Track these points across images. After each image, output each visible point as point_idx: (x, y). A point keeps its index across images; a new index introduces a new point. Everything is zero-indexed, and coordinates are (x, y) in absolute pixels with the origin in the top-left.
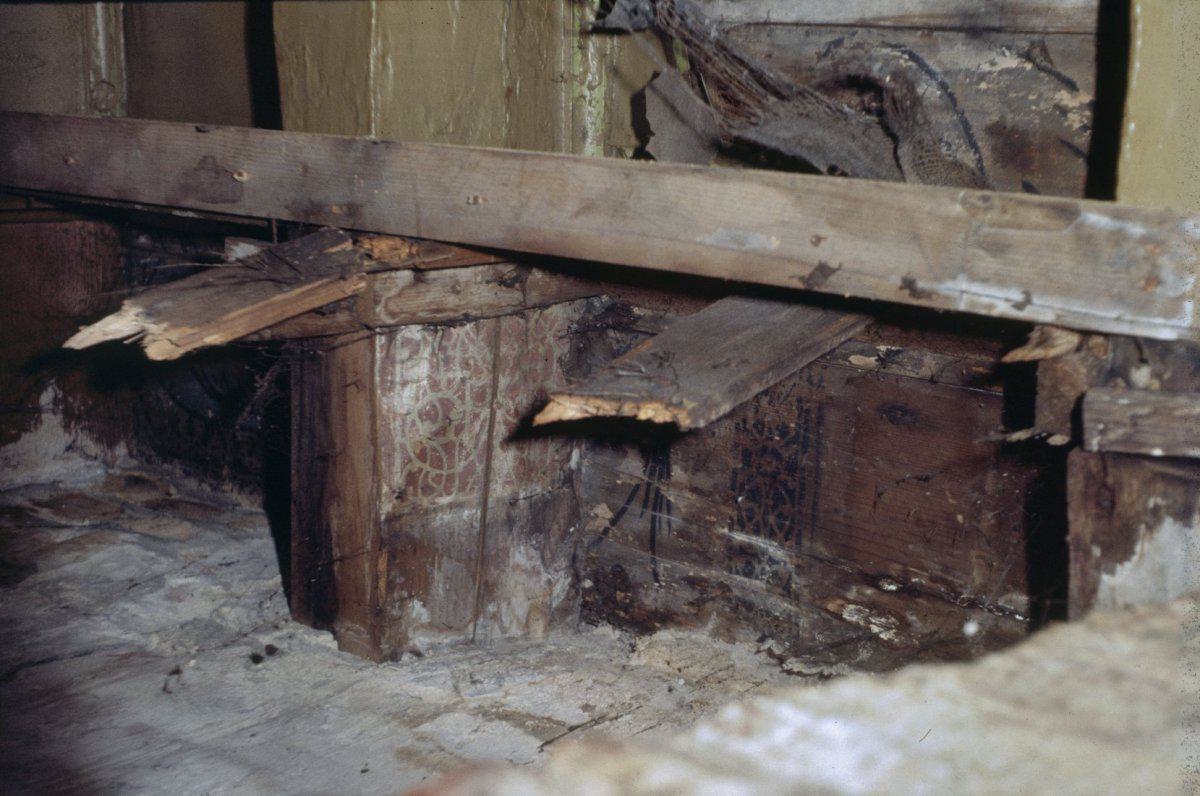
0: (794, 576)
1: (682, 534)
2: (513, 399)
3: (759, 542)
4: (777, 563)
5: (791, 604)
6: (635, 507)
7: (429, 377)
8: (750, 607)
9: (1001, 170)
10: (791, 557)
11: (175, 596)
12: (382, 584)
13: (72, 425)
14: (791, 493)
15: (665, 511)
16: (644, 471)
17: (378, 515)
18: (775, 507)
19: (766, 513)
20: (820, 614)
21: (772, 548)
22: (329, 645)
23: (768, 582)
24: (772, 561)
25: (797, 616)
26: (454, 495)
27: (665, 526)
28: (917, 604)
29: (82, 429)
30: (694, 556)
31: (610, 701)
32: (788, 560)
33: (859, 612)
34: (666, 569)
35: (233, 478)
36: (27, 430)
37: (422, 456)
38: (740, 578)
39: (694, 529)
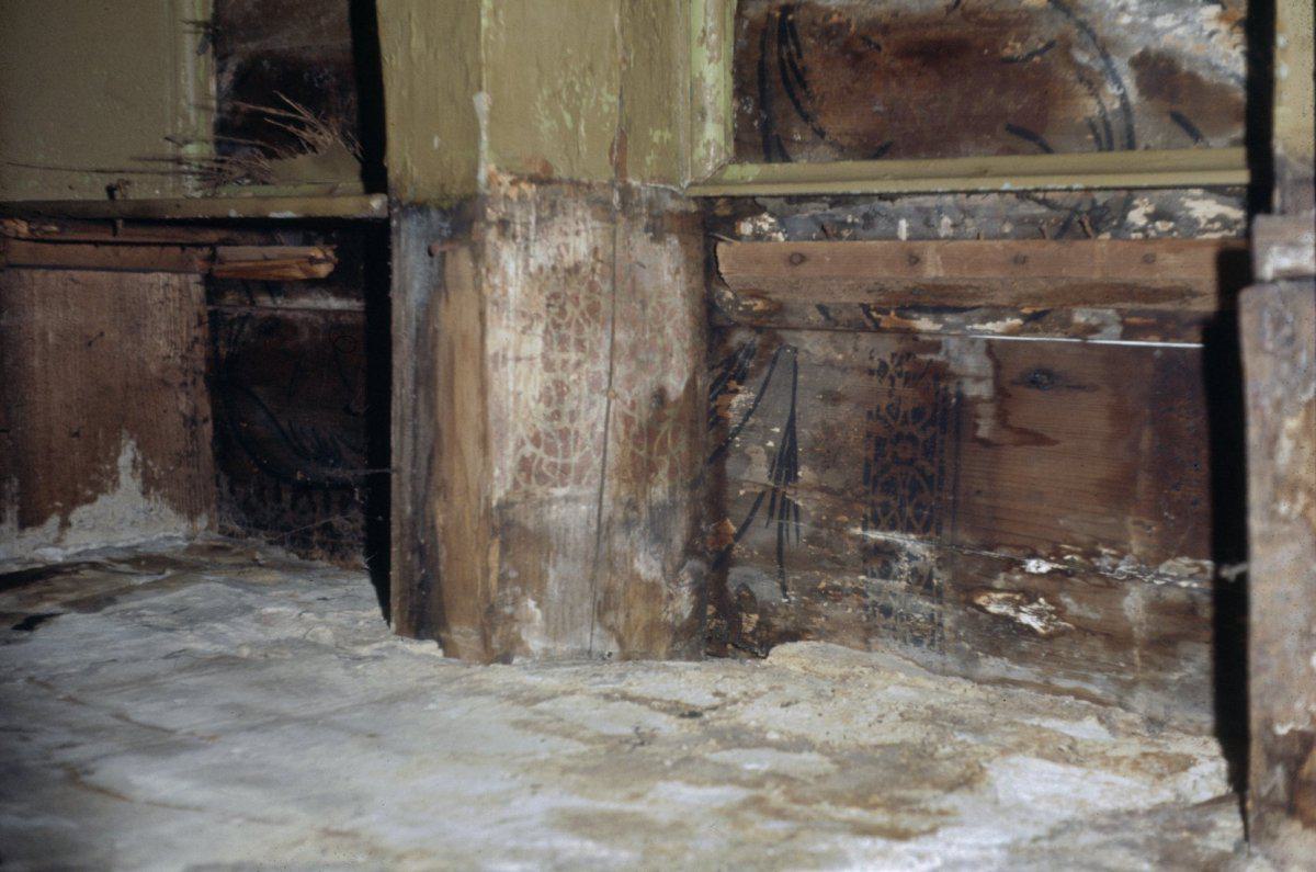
0: (935, 569)
1: (812, 539)
2: (630, 391)
3: (895, 537)
4: (917, 558)
5: (933, 603)
6: (761, 517)
7: (544, 356)
8: (887, 612)
9: (1147, 103)
10: (931, 551)
11: (266, 621)
12: (493, 577)
13: (152, 491)
14: (929, 480)
15: (793, 518)
16: (770, 477)
17: (488, 500)
18: (911, 498)
19: (902, 505)
20: (965, 610)
21: (910, 542)
22: (433, 653)
23: (908, 581)
24: (911, 557)
25: (940, 615)
26: (568, 488)
27: (793, 534)
28: (1072, 584)
29: (162, 496)
30: (826, 563)
31: (743, 688)
32: (927, 554)
33: (1006, 601)
34: (795, 581)
35: (322, 545)
36: (103, 491)
37: (536, 441)
38: (878, 581)
39: (824, 533)
